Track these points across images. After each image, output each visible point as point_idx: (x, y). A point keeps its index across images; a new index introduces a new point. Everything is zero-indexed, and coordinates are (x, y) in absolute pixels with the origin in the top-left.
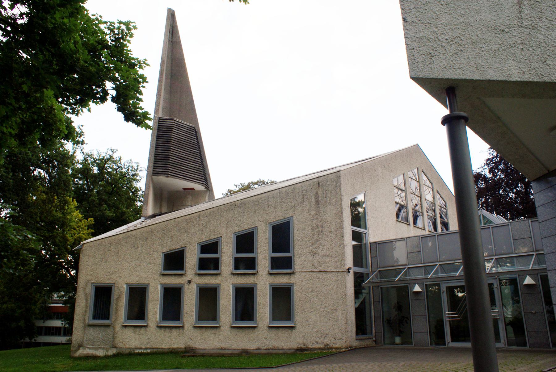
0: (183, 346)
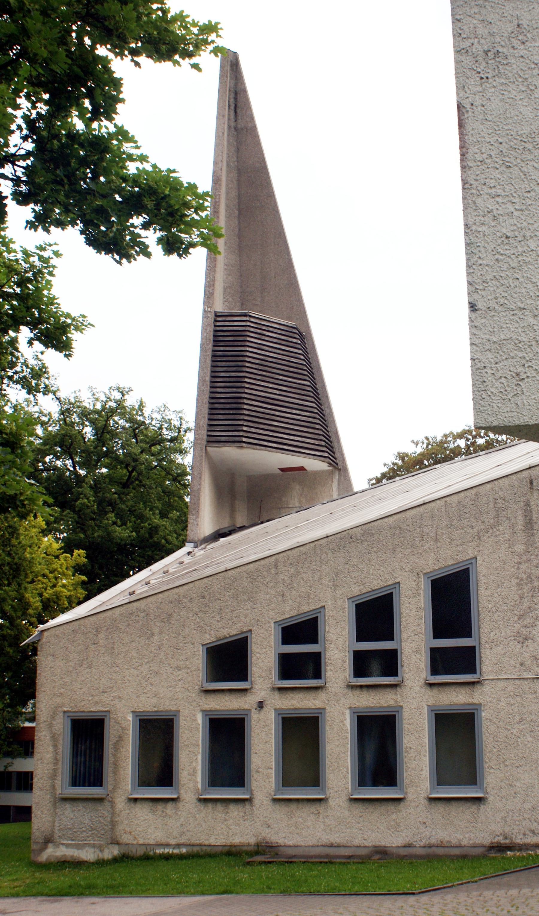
0: (252, 841)
